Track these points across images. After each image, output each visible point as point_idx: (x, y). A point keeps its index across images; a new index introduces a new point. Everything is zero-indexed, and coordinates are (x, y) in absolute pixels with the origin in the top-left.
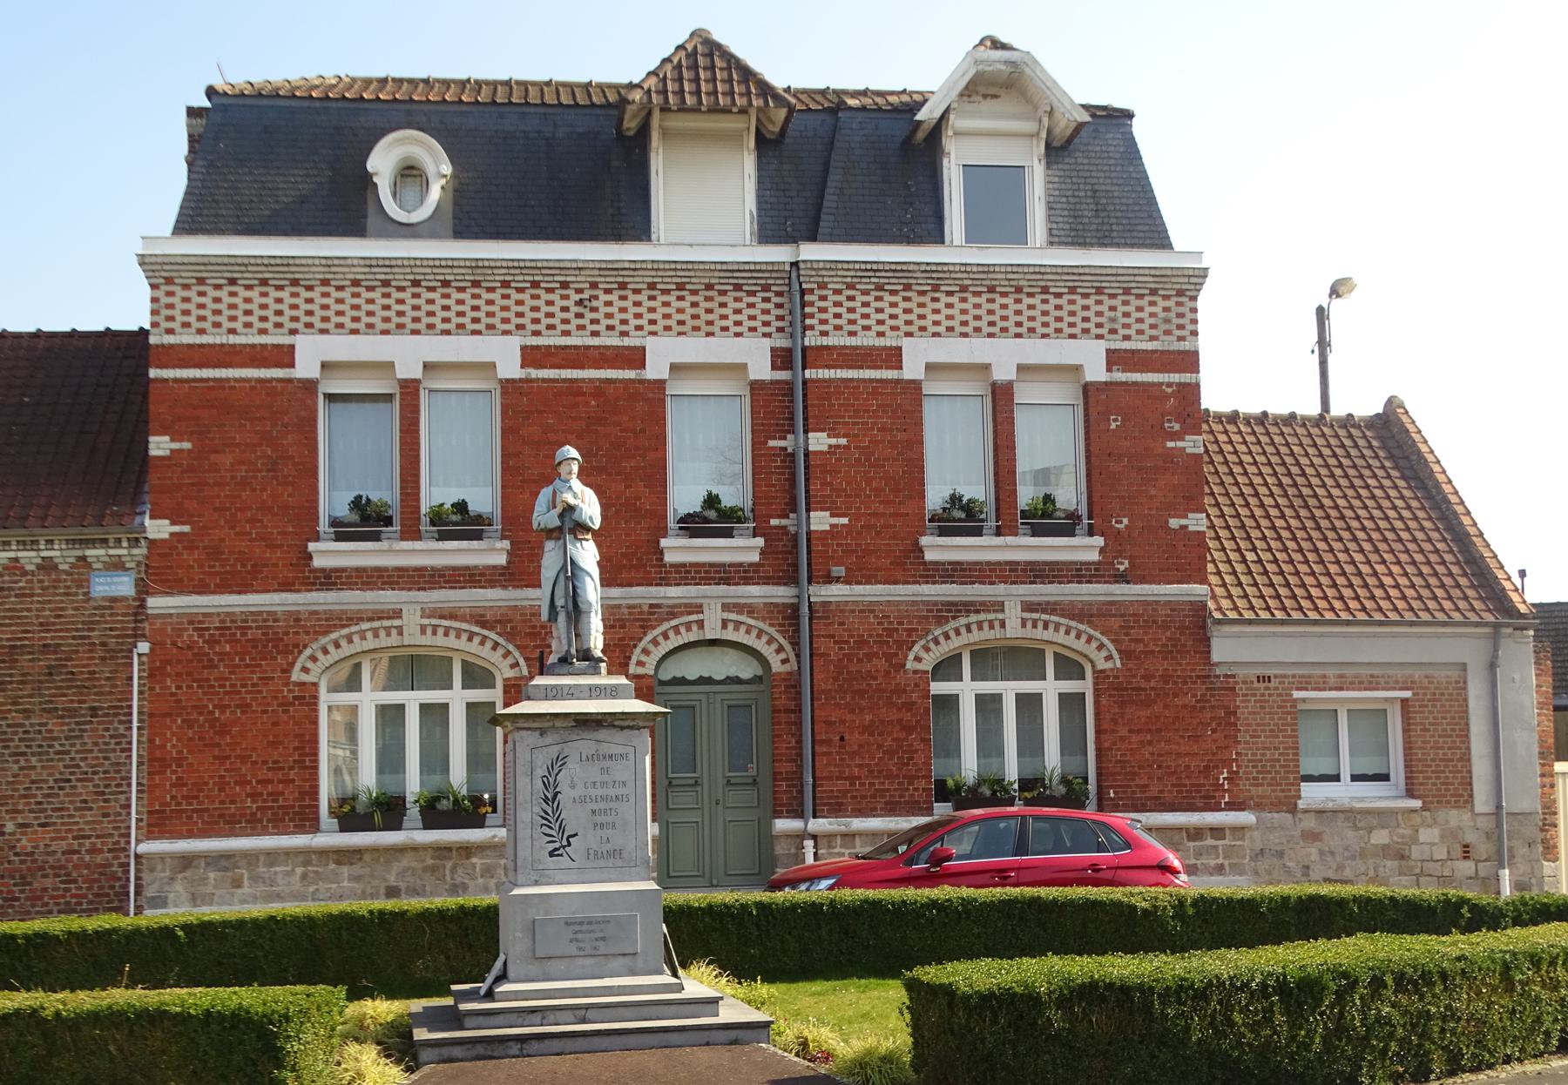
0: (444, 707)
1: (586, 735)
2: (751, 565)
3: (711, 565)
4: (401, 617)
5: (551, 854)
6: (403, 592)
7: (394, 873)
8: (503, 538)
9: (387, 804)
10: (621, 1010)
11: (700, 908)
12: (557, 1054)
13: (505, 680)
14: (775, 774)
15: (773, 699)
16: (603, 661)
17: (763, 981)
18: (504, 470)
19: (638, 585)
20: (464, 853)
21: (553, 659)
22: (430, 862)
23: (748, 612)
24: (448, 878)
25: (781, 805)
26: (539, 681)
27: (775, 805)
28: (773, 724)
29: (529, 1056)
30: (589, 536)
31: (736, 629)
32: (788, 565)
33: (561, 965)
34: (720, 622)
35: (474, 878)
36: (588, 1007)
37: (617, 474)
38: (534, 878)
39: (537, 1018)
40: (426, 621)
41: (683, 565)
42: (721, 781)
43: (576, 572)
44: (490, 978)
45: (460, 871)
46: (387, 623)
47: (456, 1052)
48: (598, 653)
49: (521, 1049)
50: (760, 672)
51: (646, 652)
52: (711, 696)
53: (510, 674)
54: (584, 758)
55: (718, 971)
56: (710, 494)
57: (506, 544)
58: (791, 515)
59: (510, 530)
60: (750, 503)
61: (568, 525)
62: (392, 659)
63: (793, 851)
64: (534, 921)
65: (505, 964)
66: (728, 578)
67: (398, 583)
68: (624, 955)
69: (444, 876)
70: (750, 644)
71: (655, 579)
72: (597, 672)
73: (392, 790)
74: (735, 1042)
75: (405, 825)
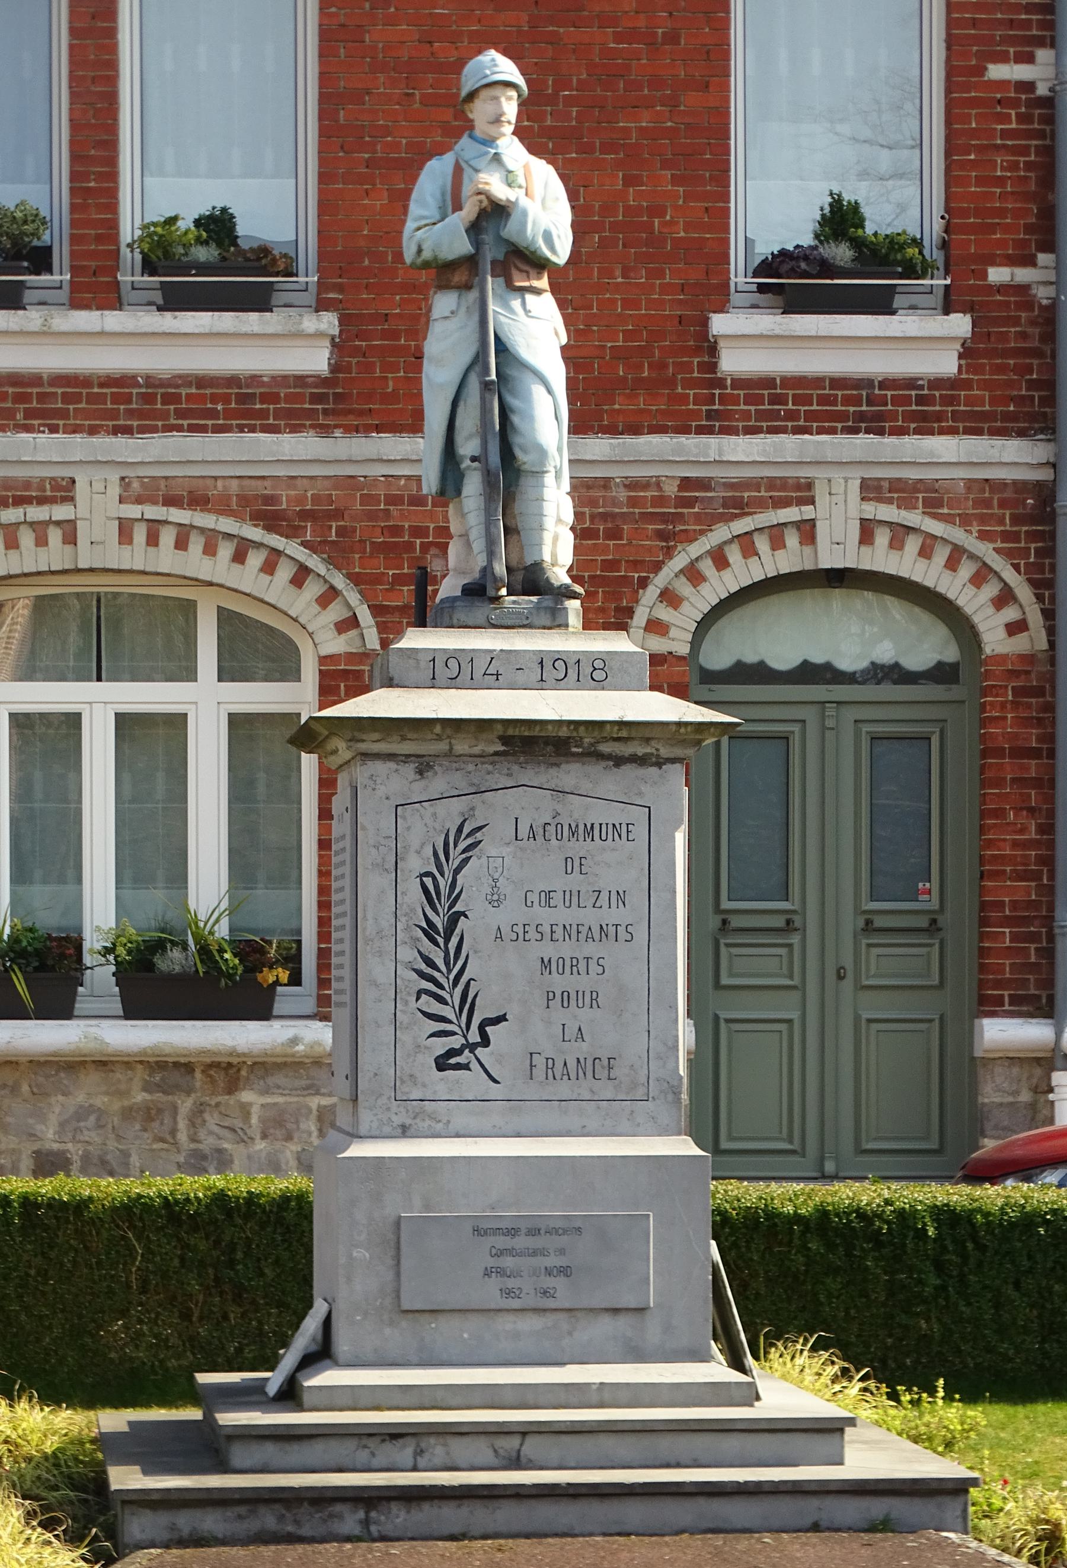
0: (177, 723)
1: (528, 775)
2: (937, 383)
3: (838, 382)
4: (71, 499)
5: (442, 1063)
6: (78, 438)
7: (53, 1120)
8: (321, 305)
9: (37, 953)
10: (607, 1443)
11: (797, 1218)
12: (453, 1538)
13: (323, 660)
14: (983, 906)
15: (984, 723)
16: (574, 596)
17: (948, 1398)
18: (326, 133)
19: (661, 430)
20: (220, 1077)
21: (448, 588)
22: (140, 1097)
23: (927, 503)
24: (182, 1137)
25: (999, 984)
26: (416, 639)
27: (982, 984)
28: (983, 784)
29: (383, 1538)
30: (543, 283)
31: (896, 544)
32: (1032, 385)
33: (465, 1330)
34: (854, 532)
35: (245, 1140)
36: (525, 1431)
37: (606, 148)
38: (397, 1120)
39: (405, 1452)
40: (133, 511)
41: (767, 382)
42: (850, 923)
43: (512, 372)
44: (289, 1359)
45: (212, 1120)
46: (37, 513)
47: (211, 1522)
48: (560, 576)
49: (366, 1523)
50: (951, 654)
51: (669, 597)
52: (831, 710)
53: (336, 645)
54: (524, 831)
55: (840, 1364)
56: (837, 203)
57: (329, 322)
58: (1043, 258)
59: (340, 288)
60: (938, 225)
61: (491, 253)
62: (42, 606)
63: (1025, 1097)
64: (398, 1222)
65: (327, 1323)
66: (880, 417)
67: (64, 414)
68: (616, 1311)
69: (173, 1132)
70: (929, 583)
71: (695, 415)
72: (556, 622)
73: (48, 920)
74: (884, 1526)
75: (80, 1006)
